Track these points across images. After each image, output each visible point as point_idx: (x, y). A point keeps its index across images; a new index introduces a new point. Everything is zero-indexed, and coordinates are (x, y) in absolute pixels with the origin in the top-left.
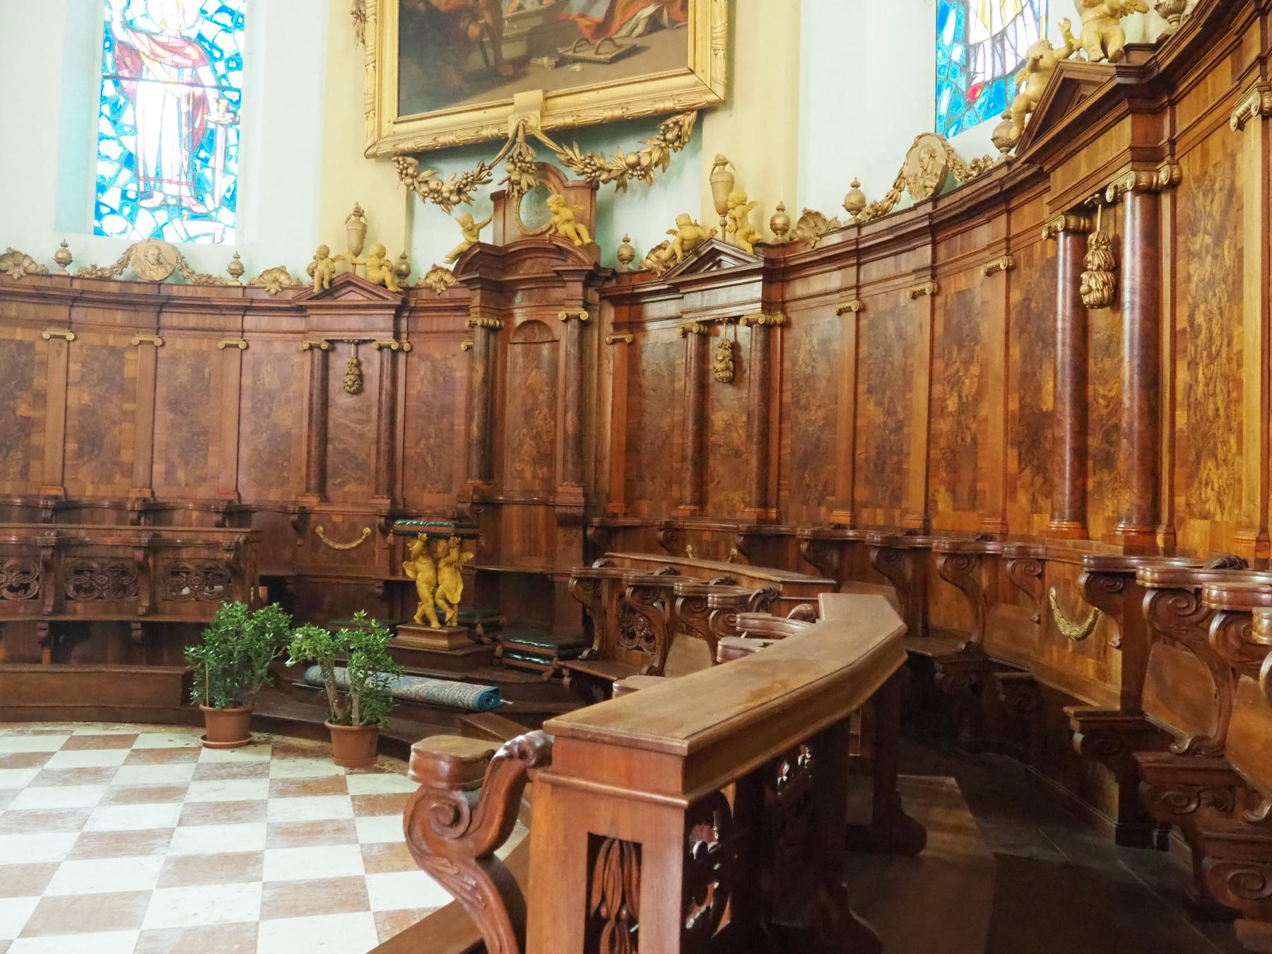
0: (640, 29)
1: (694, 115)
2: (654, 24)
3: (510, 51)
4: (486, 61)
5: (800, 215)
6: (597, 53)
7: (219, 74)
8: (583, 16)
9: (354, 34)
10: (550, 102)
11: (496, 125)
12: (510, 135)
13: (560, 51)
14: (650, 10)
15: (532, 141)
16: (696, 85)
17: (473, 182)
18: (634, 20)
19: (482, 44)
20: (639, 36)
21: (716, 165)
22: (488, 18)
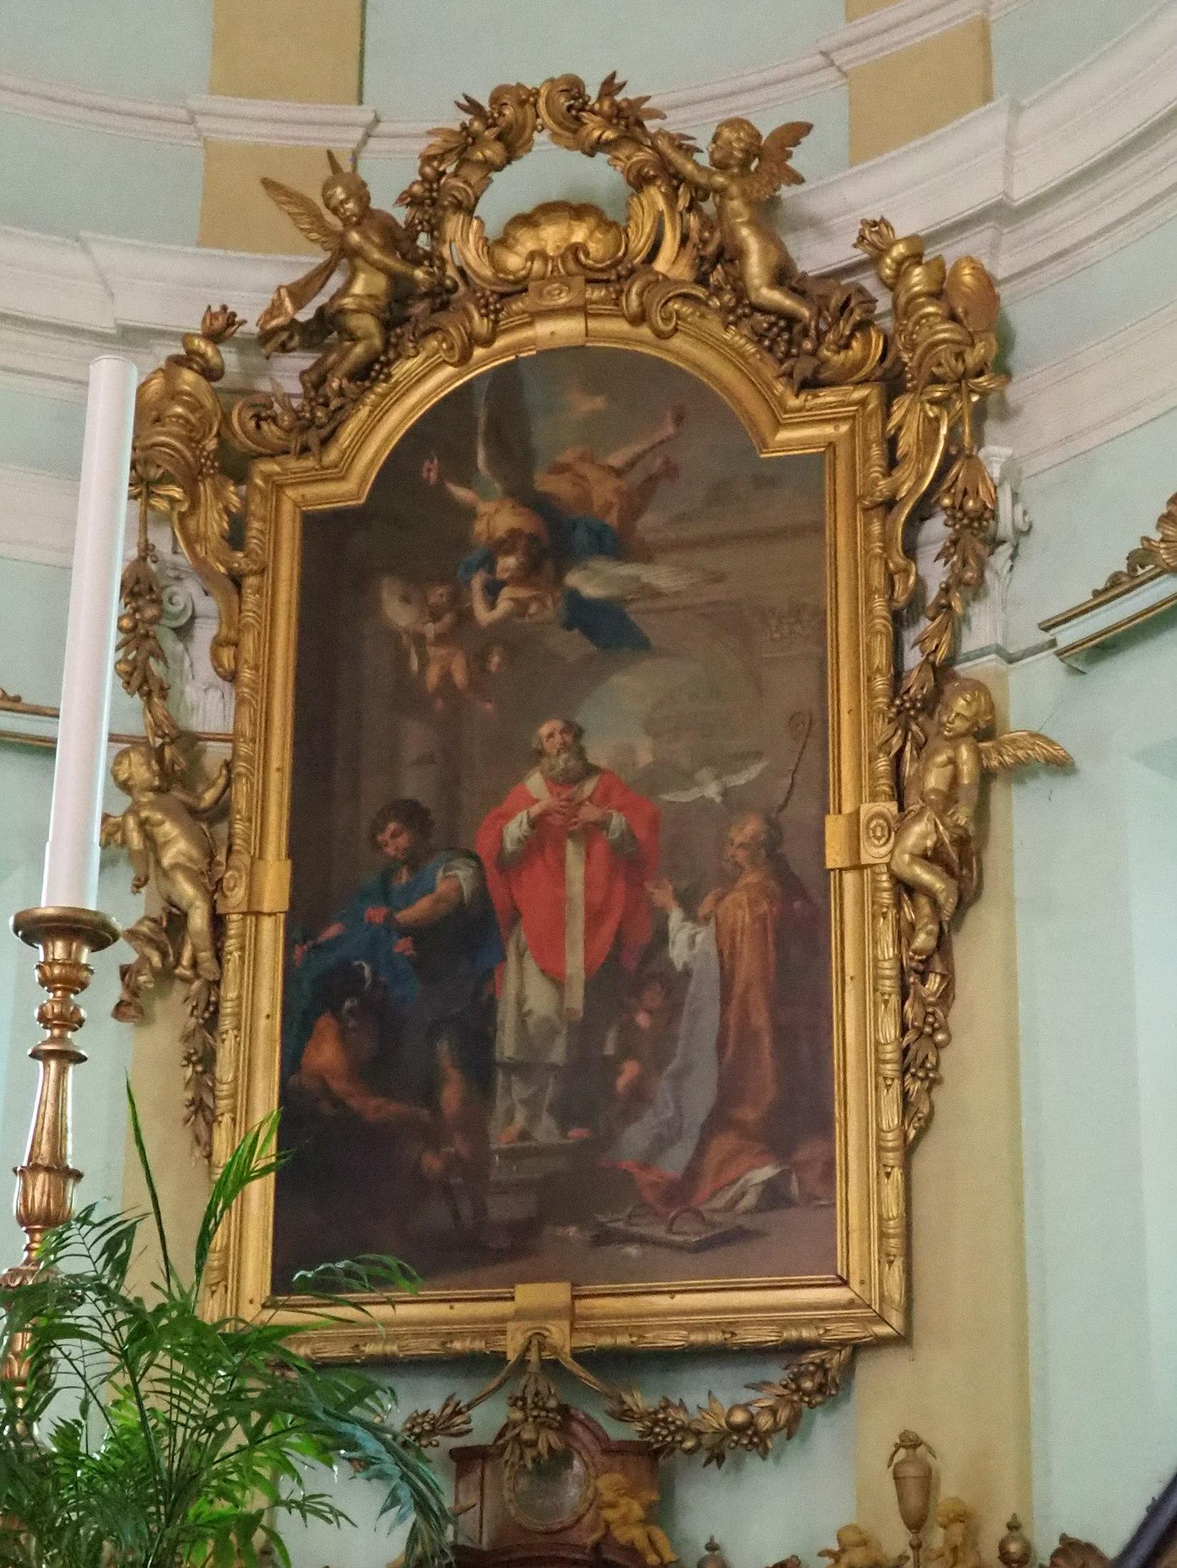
0: (749, 1200)
1: (846, 1352)
2: (774, 1196)
3: (502, 1209)
4: (456, 1216)
5: (1056, 1544)
6: (670, 1231)
7: (835, 56)
8: (646, 1166)
9: (190, 1138)
10: (578, 1303)
11: (483, 1334)
12: (512, 1357)
13: (602, 1219)
14: (766, 1172)
15: (553, 1367)
16: (851, 1304)
17: (433, 1432)
18: (735, 1189)
19: (447, 1190)
20: (747, 1212)
21: (898, 1447)
22: (459, 1146)
